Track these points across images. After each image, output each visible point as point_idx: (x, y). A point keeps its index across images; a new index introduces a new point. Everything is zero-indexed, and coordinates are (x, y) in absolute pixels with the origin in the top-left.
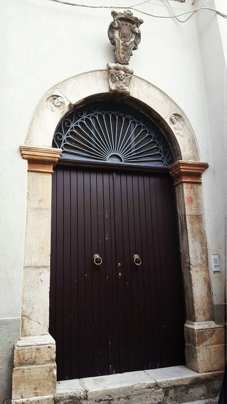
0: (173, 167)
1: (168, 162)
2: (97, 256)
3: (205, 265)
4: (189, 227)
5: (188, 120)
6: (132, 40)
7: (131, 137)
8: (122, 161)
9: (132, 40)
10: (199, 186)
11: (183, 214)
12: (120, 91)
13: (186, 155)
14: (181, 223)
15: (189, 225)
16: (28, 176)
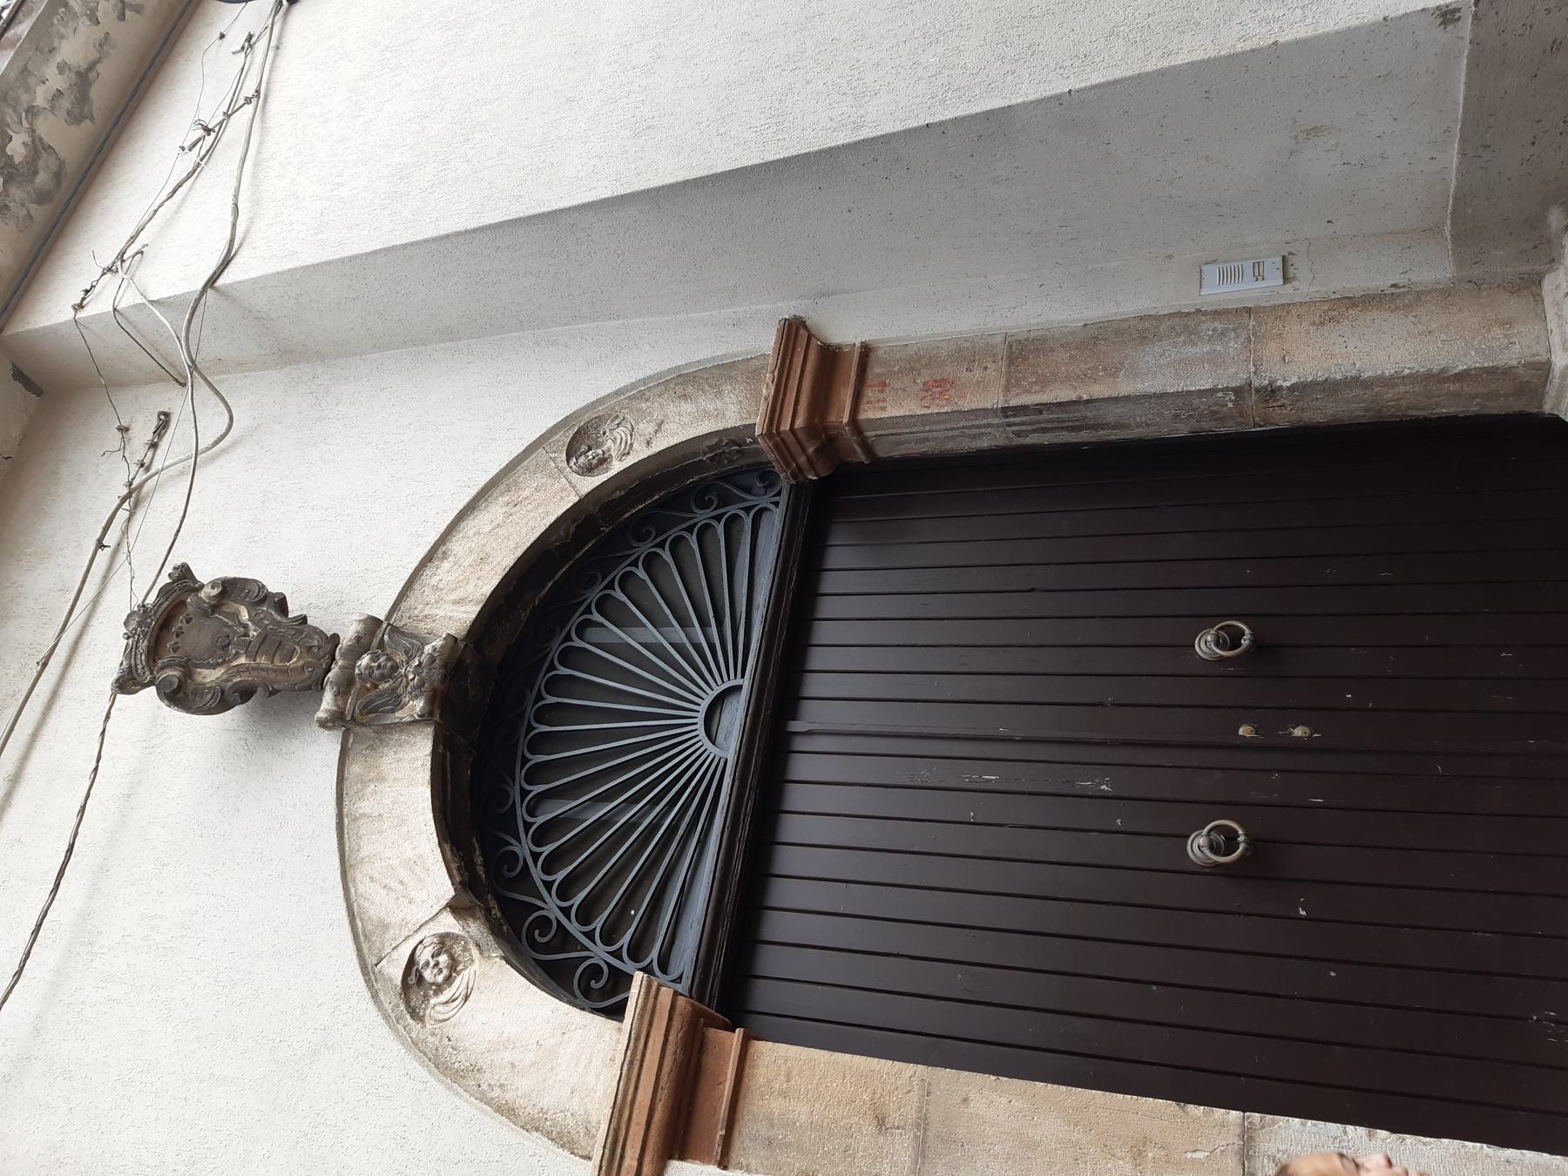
0: (788, 465)
1: (766, 487)
2: (1198, 846)
3: (1252, 323)
4: (1065, 394)
5: (600, 401)
6: (244, 615)
7: (644, 645)
8: (738, 688)
9: (244, 615)
10: (880, 352)
11: (996, 421)
12: (437, 675)
13: (733, 411)
14: (1044, 430)
15: (1054, 394)
16: (749, 1171)
